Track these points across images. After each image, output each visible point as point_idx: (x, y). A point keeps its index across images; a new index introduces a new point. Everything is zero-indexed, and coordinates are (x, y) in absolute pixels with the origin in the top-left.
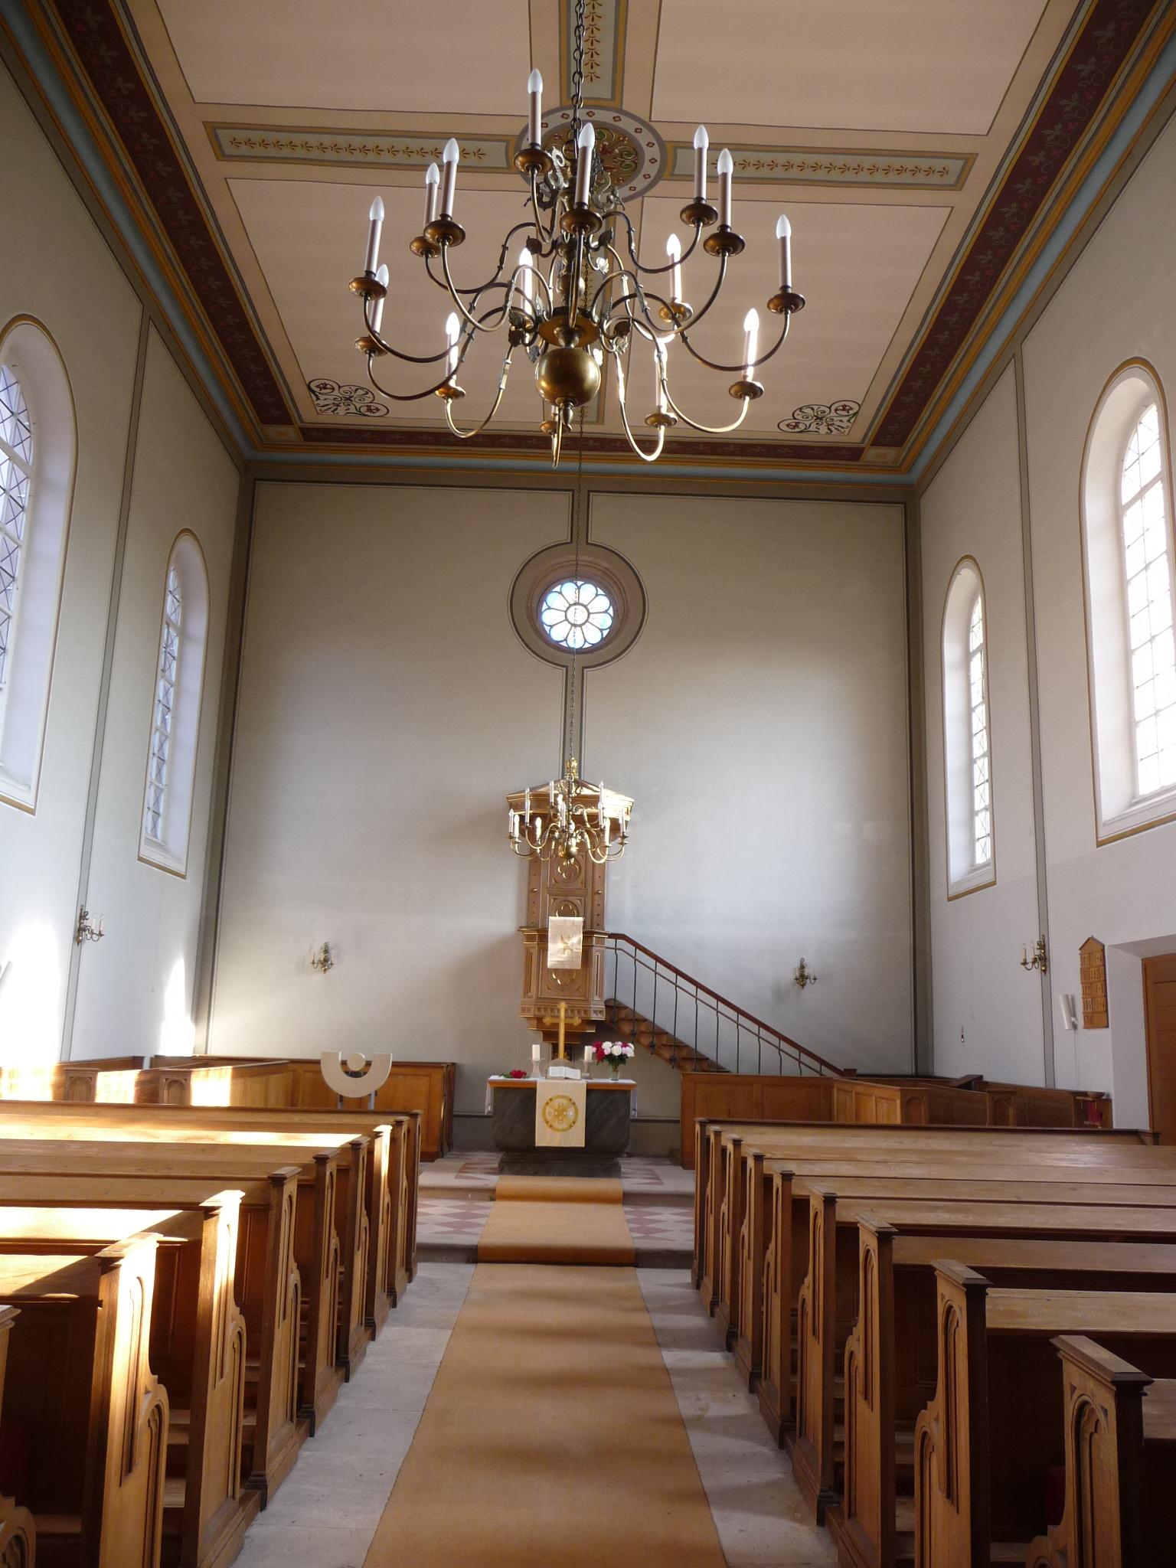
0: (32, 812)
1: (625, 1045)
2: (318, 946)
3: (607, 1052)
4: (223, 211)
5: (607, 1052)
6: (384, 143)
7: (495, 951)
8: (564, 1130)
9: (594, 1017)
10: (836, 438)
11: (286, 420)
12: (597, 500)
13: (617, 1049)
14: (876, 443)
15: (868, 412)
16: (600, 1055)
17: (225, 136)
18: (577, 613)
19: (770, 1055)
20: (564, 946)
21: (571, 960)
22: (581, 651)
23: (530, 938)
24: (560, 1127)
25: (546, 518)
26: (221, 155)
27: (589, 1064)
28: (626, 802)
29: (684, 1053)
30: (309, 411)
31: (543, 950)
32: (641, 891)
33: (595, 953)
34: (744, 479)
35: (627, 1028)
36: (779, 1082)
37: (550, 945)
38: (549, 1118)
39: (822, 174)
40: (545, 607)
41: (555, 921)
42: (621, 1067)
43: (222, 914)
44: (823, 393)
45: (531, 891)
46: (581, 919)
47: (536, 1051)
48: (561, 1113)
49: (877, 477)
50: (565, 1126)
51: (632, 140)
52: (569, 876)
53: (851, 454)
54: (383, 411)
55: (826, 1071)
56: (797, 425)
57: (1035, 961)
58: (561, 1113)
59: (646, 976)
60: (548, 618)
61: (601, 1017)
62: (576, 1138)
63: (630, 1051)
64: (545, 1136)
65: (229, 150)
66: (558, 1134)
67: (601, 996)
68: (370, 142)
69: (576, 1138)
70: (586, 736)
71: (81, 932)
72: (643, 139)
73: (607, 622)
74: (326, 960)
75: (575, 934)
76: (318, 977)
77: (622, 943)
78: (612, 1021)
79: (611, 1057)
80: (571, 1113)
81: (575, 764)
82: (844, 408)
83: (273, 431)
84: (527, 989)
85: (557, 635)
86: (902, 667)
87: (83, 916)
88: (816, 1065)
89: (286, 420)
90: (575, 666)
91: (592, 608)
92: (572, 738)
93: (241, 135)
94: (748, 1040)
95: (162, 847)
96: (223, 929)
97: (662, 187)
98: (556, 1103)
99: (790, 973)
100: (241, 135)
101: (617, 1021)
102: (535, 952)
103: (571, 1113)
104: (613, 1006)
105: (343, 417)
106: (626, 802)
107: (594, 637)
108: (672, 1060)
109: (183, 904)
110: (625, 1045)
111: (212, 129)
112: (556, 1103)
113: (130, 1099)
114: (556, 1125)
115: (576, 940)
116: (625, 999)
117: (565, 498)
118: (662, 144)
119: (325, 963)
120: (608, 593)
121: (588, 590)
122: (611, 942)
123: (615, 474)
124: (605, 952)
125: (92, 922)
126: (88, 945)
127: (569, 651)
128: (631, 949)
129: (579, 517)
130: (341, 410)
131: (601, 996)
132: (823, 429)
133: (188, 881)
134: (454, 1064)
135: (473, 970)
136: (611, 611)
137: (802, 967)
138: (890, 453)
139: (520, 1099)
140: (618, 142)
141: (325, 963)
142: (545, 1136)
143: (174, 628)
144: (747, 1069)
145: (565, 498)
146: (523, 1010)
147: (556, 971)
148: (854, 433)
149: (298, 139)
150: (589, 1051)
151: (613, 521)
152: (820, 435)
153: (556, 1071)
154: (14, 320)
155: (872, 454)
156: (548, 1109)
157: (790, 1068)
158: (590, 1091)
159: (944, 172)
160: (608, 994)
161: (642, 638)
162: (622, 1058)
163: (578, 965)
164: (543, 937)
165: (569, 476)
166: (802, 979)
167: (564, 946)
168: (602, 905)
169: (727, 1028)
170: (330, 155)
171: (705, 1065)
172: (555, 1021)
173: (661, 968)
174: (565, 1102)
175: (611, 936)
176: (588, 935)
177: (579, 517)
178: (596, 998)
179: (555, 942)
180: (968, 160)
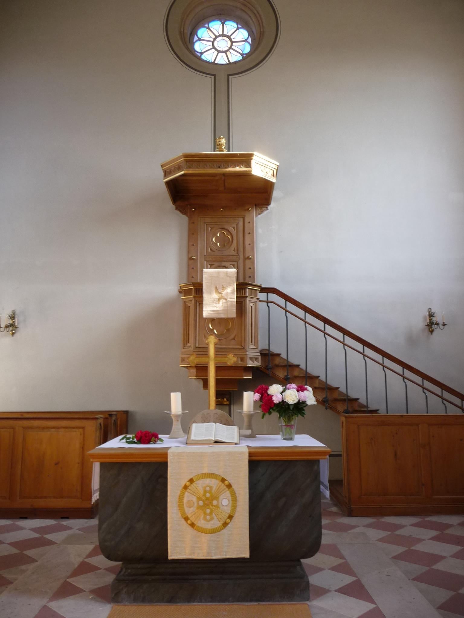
1: (300, 389)
3: (277, 399)
5: (277, 399)
7: (160, 312)
8: (214, 531)
9: (250, 364)
13: (292, 396)
16: (267, 404)
18: (222, 41)
20: (218, 302)
21: (226, 310)
23: (186, 292)
24: (208, 526)
27: (250, 417)
28: (273, 164)
31: (199, 301)
33: (249, 303)
35: (281, 374)
37: (205, 295)
38: (189, 512)
40: (196, 38)
41: (208, 272)
42: (296, 420)
45: (190, 259)
46: (234, 270)
47: (176, 402)
48: (208, 502)
50: (217, 524)
52: (223, 246)
57: (7, 327)
58: (208, 502)
59: (296, 325)
60: (202, 33)
61: (257, 364)
62: (235, 544)
64: (184, 543)
66: (205, 538)
67: (256, 344)
69: (235, 544)
74: (13, 325)
75: (229, 284)
77: (273, 297)
78: (267, 368)
79: (283, 408)
80: (225, 501)
81: (223, 141)
84: (186, 340)
89: (93, 591)
90: (222, 78)
91: (234, 37)
94: (396, 384)
98: (200, 485)
99: (419, 322)
101: (271, 368)
102: (192, 305)
103: (225, 501)
104: (266, 355)
106: (273, 164)
110: (300, 389)
112: (200, 485)
114: (201, 523)
115: (230, 292)
116: (275, 349)
119: (12, 327)
121: (230, 26)
122: (262, 296)
124: (257, 305)
128: (281, 301)
131: (256, 344)
134: (126, 412)
135: (140, 330)
136: (250, 40)
137: (431, 315)
139: (145, 484)
142: (184, 543)
144: (396, 407)
146: (183, 360)
147: (212, 320)
150: (249, 398)
153: (201, 431)
156: (187, 496)
157: (437, 407)
158: (257, 463)
160: (263, 344)
162: (300, 407)
163: (233, 314)
164: (198, 290)
166: (431, 325)
167: (218, 302)
172: (203, 360)
174: (214, 483)
175: (264, 290)
176: (241, 287)
178: (252, 346)
179: (210, 293)
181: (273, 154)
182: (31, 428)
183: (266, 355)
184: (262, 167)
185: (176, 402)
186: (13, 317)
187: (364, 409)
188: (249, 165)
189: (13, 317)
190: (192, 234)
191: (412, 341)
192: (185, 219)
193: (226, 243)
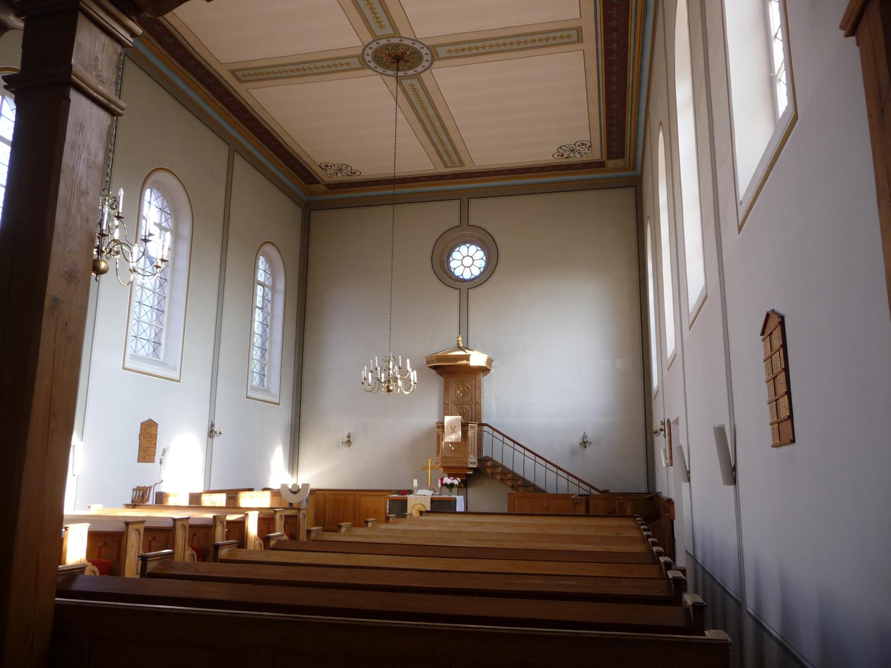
0: (179, 381)
2: (346, 434)
4: (250, 101)
6: (306, 66)
10: (585, 158)
11: (318, 182)
12: (473, 202)
14: (609, 157)
15: (597, 144)
17: (239, 74)
18: (467, 261)
19: (563, 482)
22: (471, 280)
25: (447, 214)
26: (241, 81)
29: (520, 482)
30: (326, 177)
32: (499, 401)
34: (554, 183)
36: (566, 497)
39: (509, 47)
43: (302, 420)
44: (571, 139)
47: (415, 482)
49: (620, 174)
51: (412, 48)
52: (463, 395)
53: (600, 165)
54: (358, 173)
55: (593, 491)
56: (562, 155)
60: (453, 264)
63: (456, 482)
65: (243, 79)
68: (300, 67)
70: (470, 323)
71: (211, 433)
72: (417, 46)
73: (482, 264)
76: (346, 449)
79: (446, 485)
82: (583, 144)
83: (313, 187)
85: (458, 273)
86: (635, 275)
87: (212, 425)
88: (588, 488)
89: (318, 182)
92: (464, 326)
93: (246, 72)
95: (267, 391)
96: (303, 428)
97: (436, 64)
98: (416, 507)
99: (577, 440)
100: (246, 72)
104: (482, 460)
105: (340, 178)
107: (476, 272)
108: (513, 487)
109: (282, 415)
111: (233, 72)
112: (416, 507)
113: (224, 505)
117: (457, 203)
118: (427, 47)
119: (349, 443)
120: (483, 249)
123: (481, 188)
125: (216, 429)
126: (216, 439)
127: (464, 281)
129: (464, 213)
130: (339, 175)
132: (578, 156)
133: (281, 405)
138: (620, 162)
140: (407, 50)
141: (349, 443)
143: (267, 287)
144: (551, 490)
145: (456, 203)
148: (596, 154)
149: (269, 70)
151: (482, 212)
152: (576, 158)
154: (152, 171)
155: (611, 164)
157: (574, 490)
159: (569, 36)
161: (497, 271)
165: (461, 192)
166: (584, 443)
168: (480, 409)
169: (540, 469)
170: (284, 74)
171: (531, 489)
173: (506, 440)
177: (464, 213)
180: (579, 30)
181: (483, 351)
182: (362, 495)
183: (482, 460)
184: (477, 359)
185: (415, 482)
186: (349, 437)
187: (537, 489)
188: (468, 360)
189: (349, 437)
190: (446, 388)
191: (573, 452)
192: (442, 379)
193: (465, 393)
